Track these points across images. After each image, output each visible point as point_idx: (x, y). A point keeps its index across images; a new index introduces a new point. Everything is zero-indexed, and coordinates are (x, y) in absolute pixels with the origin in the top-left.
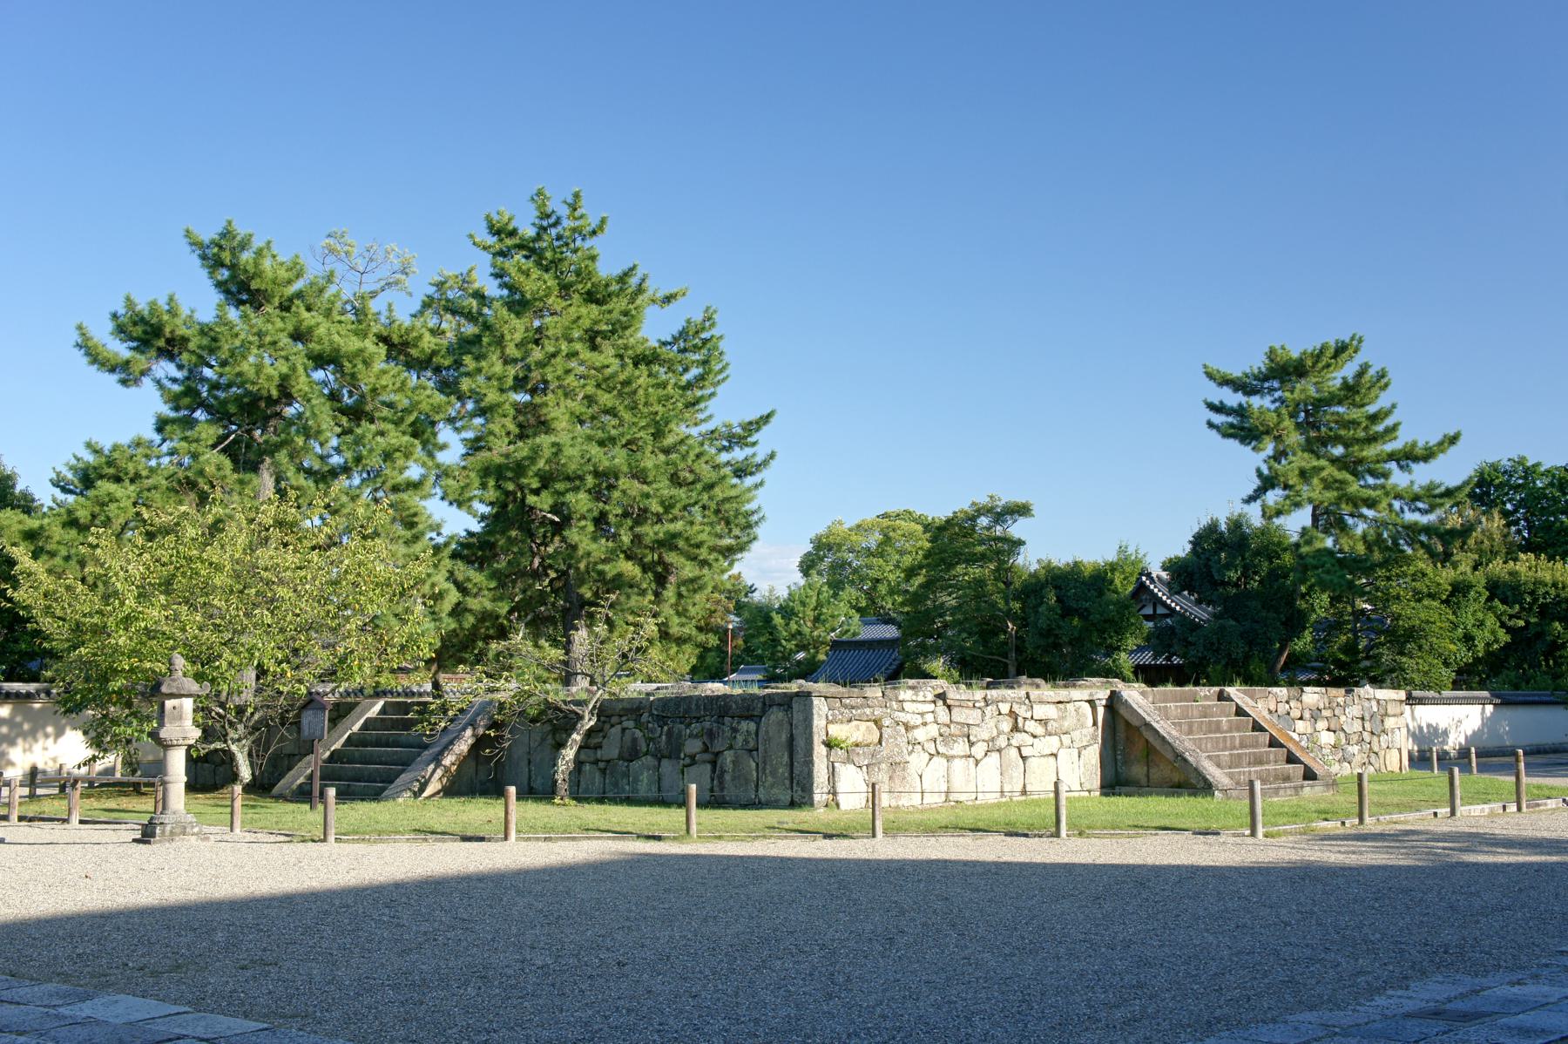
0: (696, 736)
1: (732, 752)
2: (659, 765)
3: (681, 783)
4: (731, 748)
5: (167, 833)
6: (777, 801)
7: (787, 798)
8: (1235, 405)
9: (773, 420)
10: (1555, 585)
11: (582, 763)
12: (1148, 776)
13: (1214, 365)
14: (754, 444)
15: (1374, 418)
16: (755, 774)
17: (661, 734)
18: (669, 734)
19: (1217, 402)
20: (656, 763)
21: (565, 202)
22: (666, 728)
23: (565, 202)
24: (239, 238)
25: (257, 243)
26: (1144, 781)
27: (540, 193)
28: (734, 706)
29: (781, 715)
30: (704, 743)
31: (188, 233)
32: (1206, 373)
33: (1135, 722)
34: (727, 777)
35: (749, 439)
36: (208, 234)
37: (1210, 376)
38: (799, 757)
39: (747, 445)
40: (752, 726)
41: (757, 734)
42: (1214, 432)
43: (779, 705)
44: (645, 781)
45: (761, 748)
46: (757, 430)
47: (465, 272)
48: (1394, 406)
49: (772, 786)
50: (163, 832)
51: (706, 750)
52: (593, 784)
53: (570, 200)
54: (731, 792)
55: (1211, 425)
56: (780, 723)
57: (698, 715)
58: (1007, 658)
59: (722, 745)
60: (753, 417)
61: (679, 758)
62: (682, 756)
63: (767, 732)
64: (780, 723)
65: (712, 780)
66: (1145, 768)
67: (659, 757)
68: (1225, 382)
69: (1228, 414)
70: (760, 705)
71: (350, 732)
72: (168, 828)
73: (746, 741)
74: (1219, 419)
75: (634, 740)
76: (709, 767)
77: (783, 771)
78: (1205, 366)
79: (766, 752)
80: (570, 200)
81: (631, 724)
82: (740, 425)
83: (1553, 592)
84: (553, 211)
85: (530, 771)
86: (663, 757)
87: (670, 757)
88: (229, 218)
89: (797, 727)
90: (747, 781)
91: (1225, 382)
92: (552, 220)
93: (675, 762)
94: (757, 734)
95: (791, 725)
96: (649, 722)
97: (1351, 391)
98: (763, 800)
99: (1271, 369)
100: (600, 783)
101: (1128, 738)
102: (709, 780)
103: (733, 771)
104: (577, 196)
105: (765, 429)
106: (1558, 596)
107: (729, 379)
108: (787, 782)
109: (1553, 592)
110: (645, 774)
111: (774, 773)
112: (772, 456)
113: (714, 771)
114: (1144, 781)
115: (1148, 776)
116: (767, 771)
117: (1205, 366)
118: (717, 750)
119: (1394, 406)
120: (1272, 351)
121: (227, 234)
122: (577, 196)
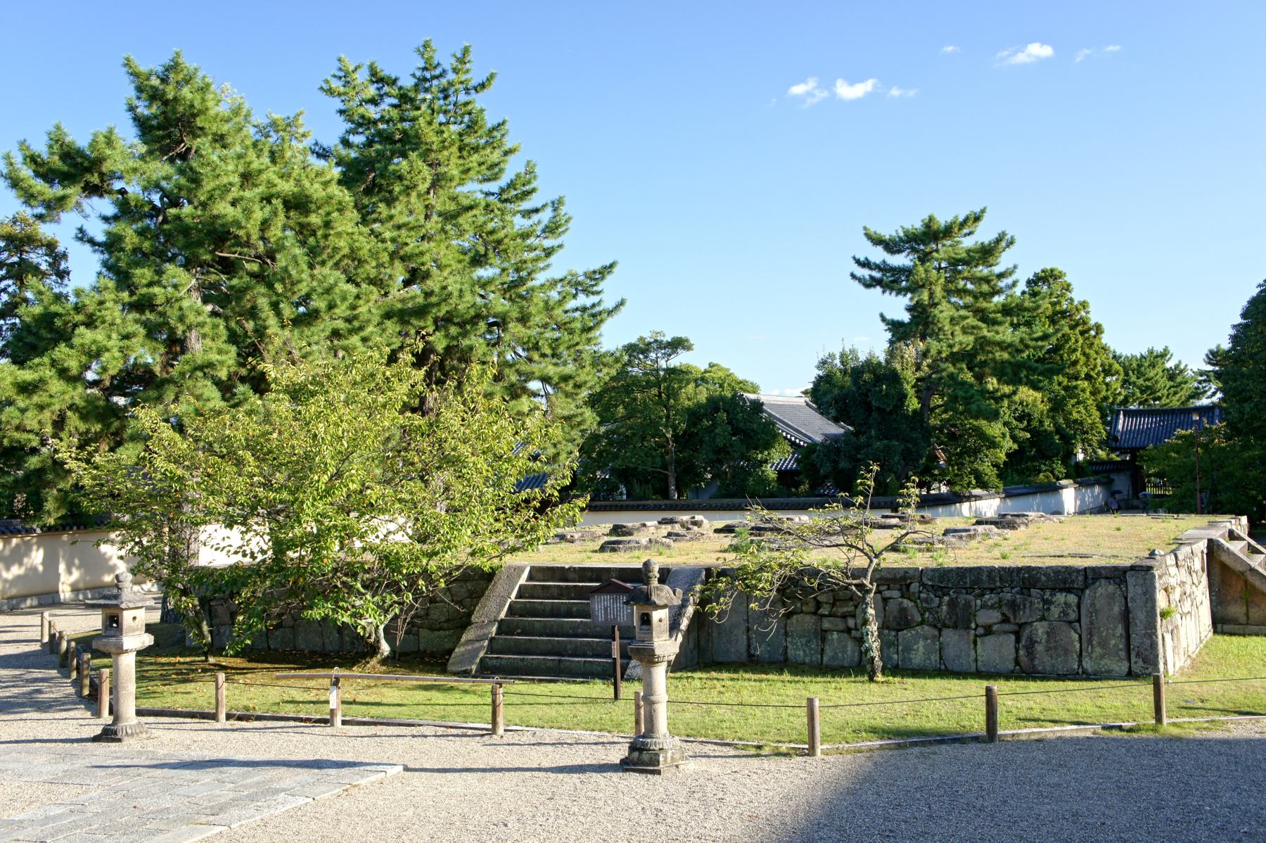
0: (992, 607)
1: (1045, 623)
2: (940, 635)
3: (973, 652)
4: (1043, 619)
5: (669, 760)
6: (1109, 671)
7: (1124, 667)
8: (878, 261)
9: (615, 270)
10: (1021, 403)
11: (826, 631)
12: (1247, 615)
13: (873, 229)
14: (598, 293)
15: (1001, 276)
16: (1078, 646)
17: (940, 605)
18: (953, 604)
19: (862, 259)
20: (937, 633)
21: (454, 56)
22: (946, 598)
23: (454, 56)
24: (185, 72)
25: (198, 81)
26: (1243, 619)
27: (426, 45)
28: (1043, 578)
29: (1111, 588)
30: (1003, 614)
31: (128, 63)
32: (866, 235)
33: (1239, 568)
34: (1039, 648)
35: (595, 289)
36: (150, 64)
37: (869, 236)
38: (1138, 630)
39: (593, 293)
40: (1072, 599)
41: (1079, 607)
42: (857, 282)
43: (1107, 578)
44: (921, 650)
45: (1083, 619)
46: (602, 278)
47: (292, 116)
48: (1015, 267)
49: (1102, 657)
50: (666, 758)
51: (1005, 620)
52: (844, 652)
53: (459, 55)
54: (1043, 659)
55: (853, 276)
56: (1111, 597)
57: (992, 586)
58: (667, 470)
59: (1031, 616)
60: (597, 266)
61: (969, 628)
62: (973, 626)
63: (1093, 604)
64: (1111, 597)
65: (1017, 650)
66: (1245, 608)
67: (939, 626)
68: (877, 241)
69: (871, 268)
70: (1081, 578)
71: (509, 600)
72: (669, 754)
73: (1065, 613)
74: (865, 273)
75: (903, 610)
76: (1013, 637)
77: (1116, 642)
78: (865, 228)
79: (1092, 623)
80: (459, 55)
81: (896, 594)
82: (585, 274)
83: (1020, 408)
84: (438, 64)
85: (749, 639)
86: (945, 626)
87: (955, 627)
88: (178, 50)
89: (1133, 600)
90: (1067, 652)
91: (877, 241)
92: (437, 72)
93: (962, 632)
94: (1079, 607)
95: (1126, 598)
96: (920, 592)
97: (987, 253)
98: (1090, 670)
99: (924, 233)
100: (853, 652)
101: (1223, 581)
102: (1013, 650)
103: (1048, 641)
104: (466, 51)
105: (609, 278)
106: (1023, 411)
107: (568, 232)
108: (1123, 654)
109: (1020, 408)
110: (921, 643)
111: (1103, 644)
112: (622, 303)
113: (1018, 641)
114: (1243, 619)
115: (1247, 615)
116: (1094, 643)
117: (865, 228)
118: (1022, 621)
119: (1015, 267)
120: (931, 219)
121: (174, 67)
122: (466, 51)
